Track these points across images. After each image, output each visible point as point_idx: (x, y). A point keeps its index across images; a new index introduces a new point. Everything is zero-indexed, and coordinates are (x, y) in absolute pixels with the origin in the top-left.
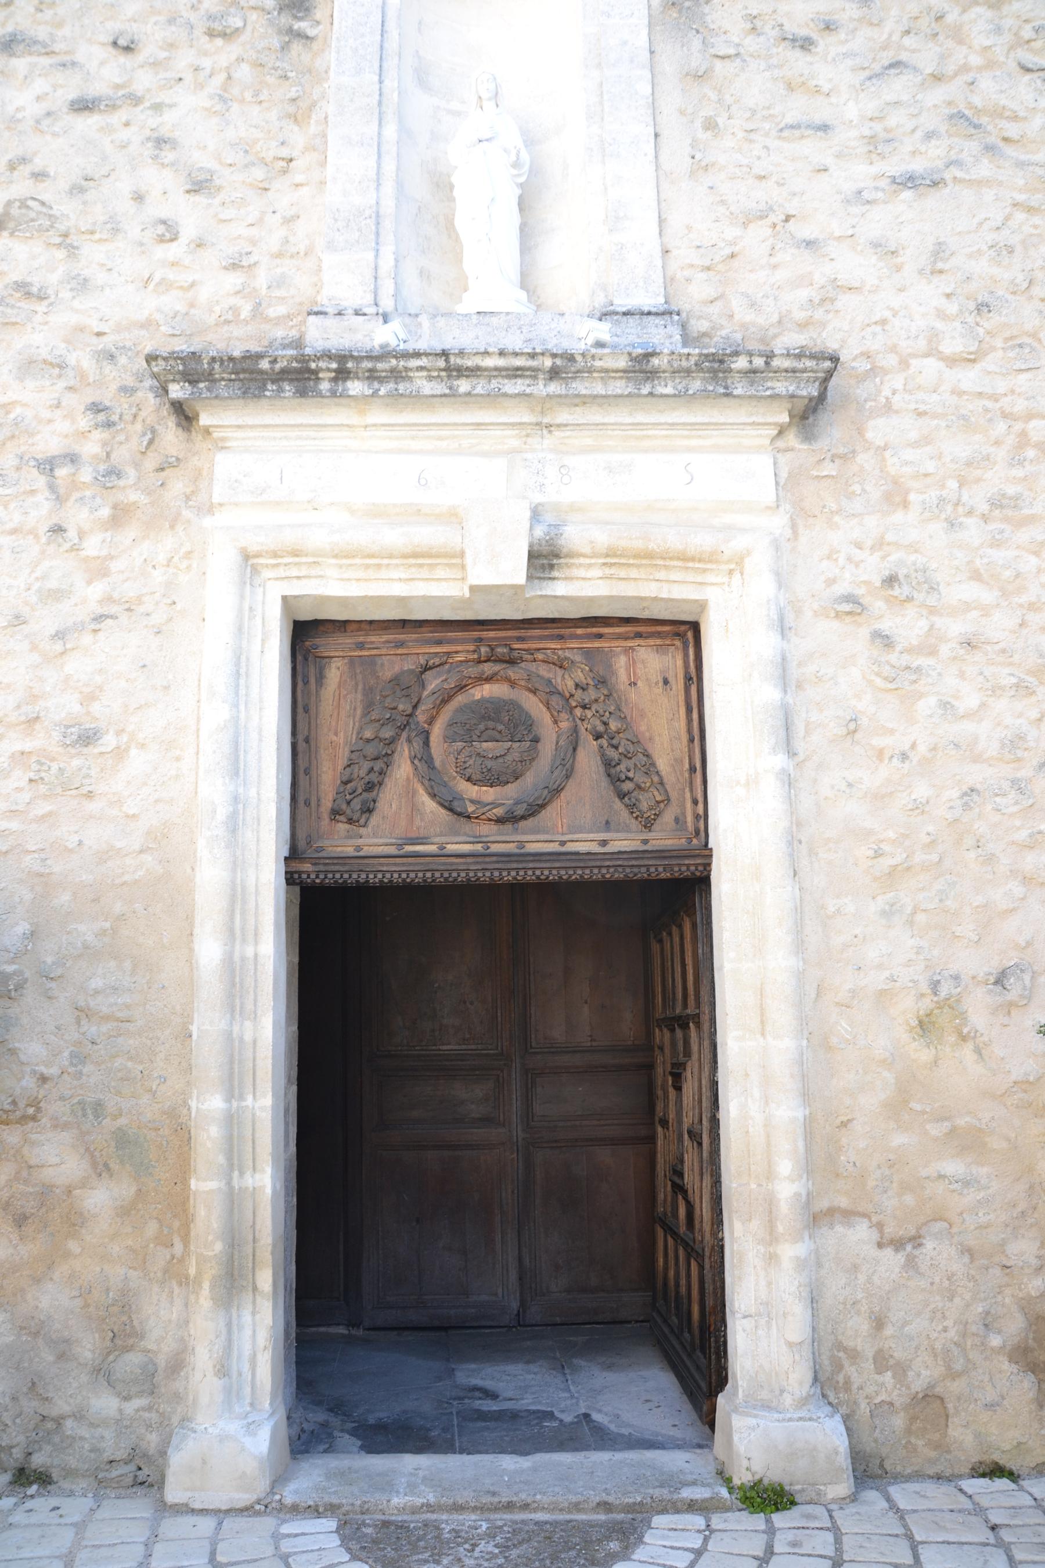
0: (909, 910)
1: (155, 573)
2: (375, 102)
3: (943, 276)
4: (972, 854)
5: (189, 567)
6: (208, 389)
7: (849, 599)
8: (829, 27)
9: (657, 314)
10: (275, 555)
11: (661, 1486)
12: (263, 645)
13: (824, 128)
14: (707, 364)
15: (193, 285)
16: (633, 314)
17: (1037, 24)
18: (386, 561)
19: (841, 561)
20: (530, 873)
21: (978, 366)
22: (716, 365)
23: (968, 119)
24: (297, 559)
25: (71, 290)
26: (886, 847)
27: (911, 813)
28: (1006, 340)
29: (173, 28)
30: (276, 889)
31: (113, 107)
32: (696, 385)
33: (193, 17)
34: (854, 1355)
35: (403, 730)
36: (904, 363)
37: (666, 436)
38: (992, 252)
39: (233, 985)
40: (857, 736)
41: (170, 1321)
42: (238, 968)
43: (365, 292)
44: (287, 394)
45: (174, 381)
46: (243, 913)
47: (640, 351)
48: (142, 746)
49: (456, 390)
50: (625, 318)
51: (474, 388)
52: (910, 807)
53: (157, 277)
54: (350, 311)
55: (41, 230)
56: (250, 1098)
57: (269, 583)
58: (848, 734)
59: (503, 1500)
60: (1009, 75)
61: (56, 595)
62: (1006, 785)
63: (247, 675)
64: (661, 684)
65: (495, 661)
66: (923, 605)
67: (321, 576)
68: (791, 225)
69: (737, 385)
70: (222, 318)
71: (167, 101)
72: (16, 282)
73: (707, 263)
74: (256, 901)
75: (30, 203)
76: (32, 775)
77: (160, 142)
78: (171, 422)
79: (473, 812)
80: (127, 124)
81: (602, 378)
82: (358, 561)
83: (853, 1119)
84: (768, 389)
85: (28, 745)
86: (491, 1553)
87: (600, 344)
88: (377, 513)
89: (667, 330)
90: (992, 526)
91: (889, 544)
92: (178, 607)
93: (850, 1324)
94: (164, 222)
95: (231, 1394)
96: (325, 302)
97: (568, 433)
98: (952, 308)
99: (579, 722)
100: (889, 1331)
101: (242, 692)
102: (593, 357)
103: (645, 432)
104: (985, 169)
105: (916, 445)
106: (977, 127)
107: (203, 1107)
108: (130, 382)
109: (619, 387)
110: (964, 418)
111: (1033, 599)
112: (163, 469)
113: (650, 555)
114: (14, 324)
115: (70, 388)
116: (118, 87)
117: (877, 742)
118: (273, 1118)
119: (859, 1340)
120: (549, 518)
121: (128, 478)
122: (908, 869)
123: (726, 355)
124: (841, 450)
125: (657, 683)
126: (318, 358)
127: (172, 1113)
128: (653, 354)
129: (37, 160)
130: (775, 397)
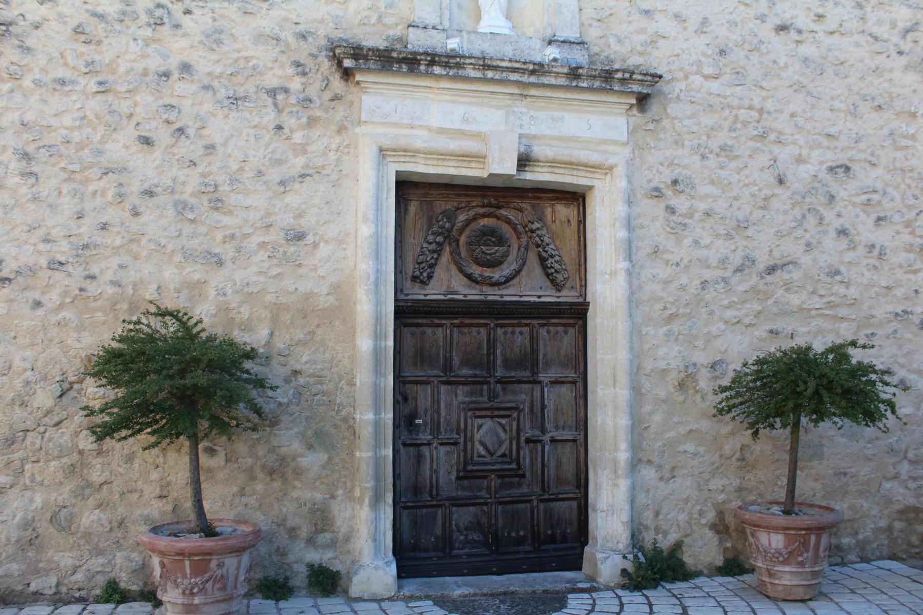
0: (676, 334)
1: (331, 154)
3: (705, 35)
4: (704, 310)
5: (348, 153)
7: (657, 189)
10: (395, 150)
18: (448, 157)
21: (718, 81)
24: (405, 153)
26: (668, 305)
28: (732, 69)
32: (597, 84)
34: (647, 528)
36: (686, 77)
40: (658, 254)
41: (345, 518)
47: (574, 65)
48: (327, 242)
50: (562, 45)
51: (494, 75)
54: (430, 27)
61: (280, 162)
62: (720, 279)
66: (689, 194)
73: (599, 18)
85: (266, 239)
87: (555, 60)
88: (442, 131)
92: (344, 172)
93: (645, 514)
98: (709, 52)
100: (661, 517)
102: (552, 66)
105: (689, 117)
108: (315, 51)
109: (562, 81)
110: (711, 106)
111: (736, 195)
113: (571, 164)
115: (282, 52)
117: (667, 257)
122: (677, 315)
124: (656, 118)
127: (345, 420)
128: (581, 68)
130: (632, 92)
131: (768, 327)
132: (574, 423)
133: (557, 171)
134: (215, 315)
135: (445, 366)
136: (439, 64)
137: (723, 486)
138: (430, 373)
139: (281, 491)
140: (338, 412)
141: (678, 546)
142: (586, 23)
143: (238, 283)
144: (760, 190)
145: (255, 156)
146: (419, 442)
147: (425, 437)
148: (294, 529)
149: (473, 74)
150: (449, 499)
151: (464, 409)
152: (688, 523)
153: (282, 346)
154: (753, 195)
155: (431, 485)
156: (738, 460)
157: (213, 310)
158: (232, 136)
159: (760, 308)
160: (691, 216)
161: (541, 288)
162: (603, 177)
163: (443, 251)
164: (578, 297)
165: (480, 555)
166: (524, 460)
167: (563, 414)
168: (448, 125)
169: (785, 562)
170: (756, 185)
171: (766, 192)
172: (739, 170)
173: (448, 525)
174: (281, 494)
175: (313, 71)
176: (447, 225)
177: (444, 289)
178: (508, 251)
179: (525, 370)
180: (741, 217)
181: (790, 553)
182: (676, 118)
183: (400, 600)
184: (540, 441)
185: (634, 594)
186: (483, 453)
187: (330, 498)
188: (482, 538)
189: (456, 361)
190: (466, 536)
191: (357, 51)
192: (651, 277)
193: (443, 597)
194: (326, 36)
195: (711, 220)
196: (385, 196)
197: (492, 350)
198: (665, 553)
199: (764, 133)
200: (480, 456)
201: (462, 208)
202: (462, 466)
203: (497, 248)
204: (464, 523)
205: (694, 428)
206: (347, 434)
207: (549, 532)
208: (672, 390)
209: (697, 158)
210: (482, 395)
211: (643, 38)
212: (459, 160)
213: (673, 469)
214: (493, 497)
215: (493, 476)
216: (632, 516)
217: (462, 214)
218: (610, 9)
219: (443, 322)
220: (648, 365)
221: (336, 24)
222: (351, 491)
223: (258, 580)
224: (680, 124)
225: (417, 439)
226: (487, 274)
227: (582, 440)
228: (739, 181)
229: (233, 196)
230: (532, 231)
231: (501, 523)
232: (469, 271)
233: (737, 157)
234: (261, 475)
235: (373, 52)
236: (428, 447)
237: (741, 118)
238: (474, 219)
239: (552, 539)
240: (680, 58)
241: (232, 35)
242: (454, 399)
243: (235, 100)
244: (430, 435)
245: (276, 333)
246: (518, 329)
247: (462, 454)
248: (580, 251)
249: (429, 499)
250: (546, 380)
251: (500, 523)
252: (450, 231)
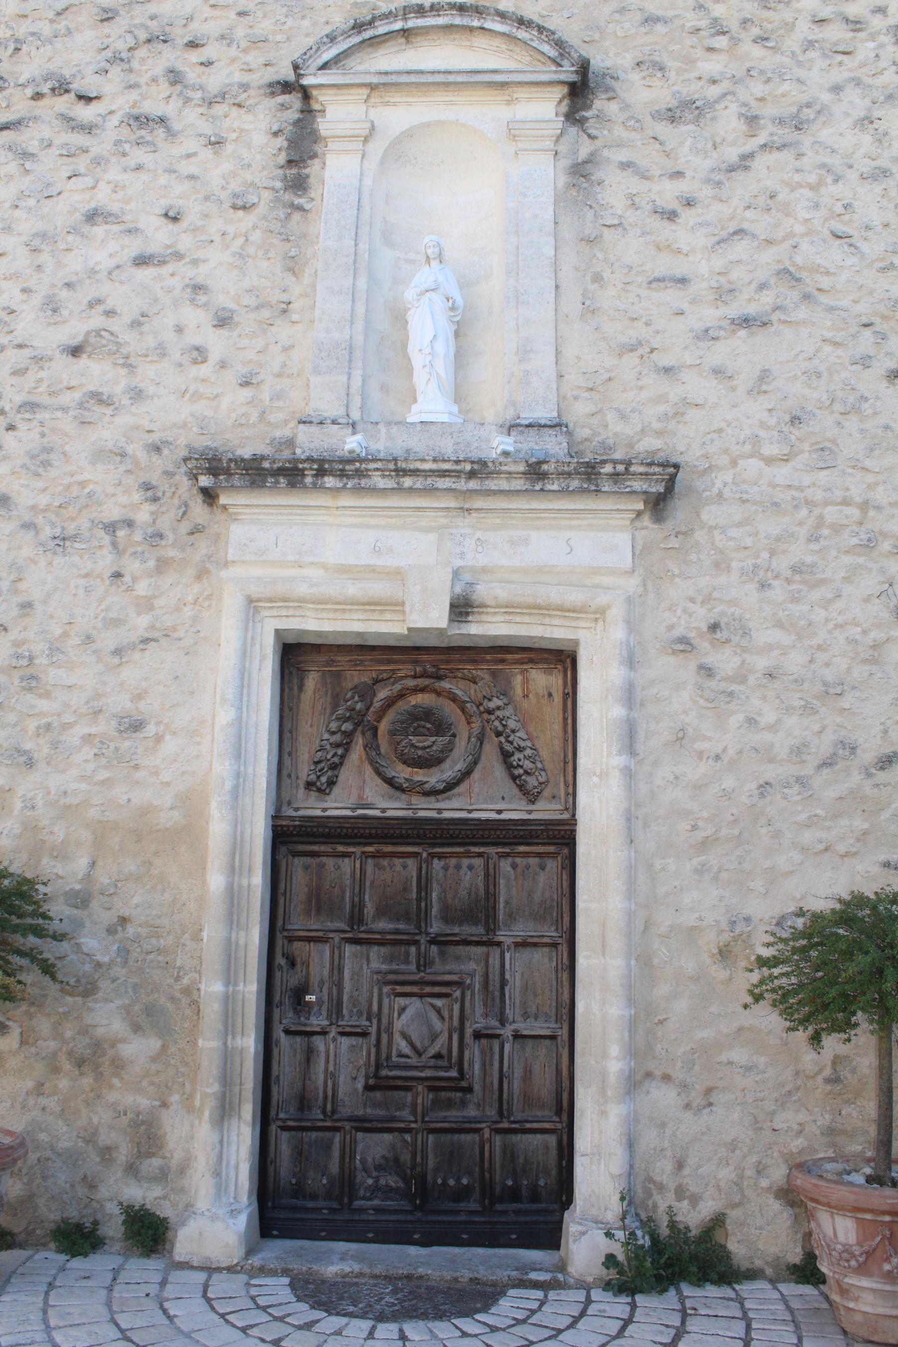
0: (715, 869)
1: (186, 609)
2: (352, 261)
4: (764, 831)
5: (210, 606)
6: (227, 480)
7: (683, 640)
8: (689, 203)
9: (550, 426)
13: (682, 281)
15: (217, 396)
17: (845, 202)
18: (349, 607)
19: (679, 613)
21: (790, 464)
22: (590, 470)
23: (791, 274)
25: (131, 398)
26: (700, 823)
28: (812, 445)
29: (208, 204)
30: (265, 839)
31: (162, 263)
32: (575, 484)
33: (224, 195)
34: (661, 1187)
36: (734, 463)
37: (555, 518)
38: (804, 377)
39: (232, 905)
40: (684, 742)
41: (181, 1138)
47: (534, 460)
48: (174, 733)
50: (527, 430)
51: (414, 483)
53: (191, 391)
54: (329, 421)
55: (111, 353)
56: (242, 984)
60: (824, 240)
61: (115, 623)
63: (249, 686)
68: (654, 356)
71: (202, 257)
72: (91, 392)
73: (591, 386)
75: (103, 333)
76: (96, 751)
77: (198, 288)
78: (199, 499)
80: (172, 275)
82: (328, 606)
85: (93, 730)
87: (506, 454)
88: (343, 570)
90: (793, 587)
92: (202, 634)
94: (197, 349)
95: (220, 1189)
96: (311, 413)
98: (773, 421)
100: (687, 1171)
101: (245, 699)
102: (500, 463)
104: (802, 313)
105: (739, 525)
106: (798, 280)
108: (171, 468)
109: (519, 484)
110: (776, 504)
111: (821, 642)
112: (192, 533)
113: (538, 607)
114: (90, 423)
115: (129, 472)
116: (168, 247)
117: (700, 746)
118: (258, 1000)
120: (467, 577)
122: (717, 839)
124: (684, 529)
129: (108, 301)
130: (633, 492)
131: (882, 858)
132: (554, 1009)
133: (518, 619)
134: (20, 836)
135: (352, 917)
136: (331, 473)
137: (800, 1124)
138: (330, 925)
139: (92, 1090)
140: (178, 979)
141: (718, 1221)
142: (569, 395)
143: (53, 792)
144: (865, 632)
145: (83, 616)
146: (308, 1029)
147: (318, 1021)
148: (108, 1149)
149: (381, 483)
150: (350, 1119)
151: (378, 981)
152: (736, 1184)
153: (106, 881)
154: (852, 641)
156: (828, 1081)
157: (17, 830)
158: (56, 589)
159: (866, 826)
160: (742, 679)
161: (503, 798)
162: (592, 625)
163: (353, 745)
164: (561, 812)
165: (396, 1212)
166: (471, 1063)
167: (536, 996)
168: (352, 561)
169: (862, 1270)
170: (857, 625)
171: (876, 635)
172: (826, 604)
173: (347, 1160)
174: (92, 1095)
175: (168, 494)
176: (359, 706)
177: (353, 800)
178: (451, 742)
179: (476, 924)
180: (829, 678)
181: (869, 1254)
182: (716, 527)
184: (498, 1036)
186: (405, 1048)
188: (401, 1185)
189: (370, 908)
190: (377, 1179)
191: (214, 464)
192: (672, 778)
193: (311, 1274)
194: (188, 446)
195: (777, 684)
196: (256, 665)
197: (423, 894)
198: (694, 1233)
199: (869, 540)
200: (401, 1055)
201: (383, 680)
202: (372, 1069)
203: (433, 739)
204: (374, 1159)
205: (747, 1025)
206: (188, 1012)
207: (510, 1183)
208: (708, 961)
209: (752, 587)
210: (407, 962)
211: (661, 408)
212: (366, 611)
213: (709, 1091)
214: (419, 1119)
215: (420, 1088)
216: (631, 1166)
218: (608, 371)
219: (351, 849)
220: (665, 920)
222: (190, 1098)
223: (53, 1221)
224: (722, 536)
225: (305, 1025)
226: (417, 778)
227: (566, 1037)
228: (827, 620)
229: (52, 671)
230: (490, 712)
231: (431, 1163)
232: (390, 773)
233: (823, 582)
234: (67, 1066)
236: (322, 1037)
237: (829, 519)
238: (401, 696)
239: (514, 1195)
240: (723, 435)
241: (64, 454)
242: (365, 966)
243: (62, 540)
245: (100, 863)
246: (465, 862)
247: (373, 1050)
249: (321, 1117)
250: (508, 941)
252: (363, 714)
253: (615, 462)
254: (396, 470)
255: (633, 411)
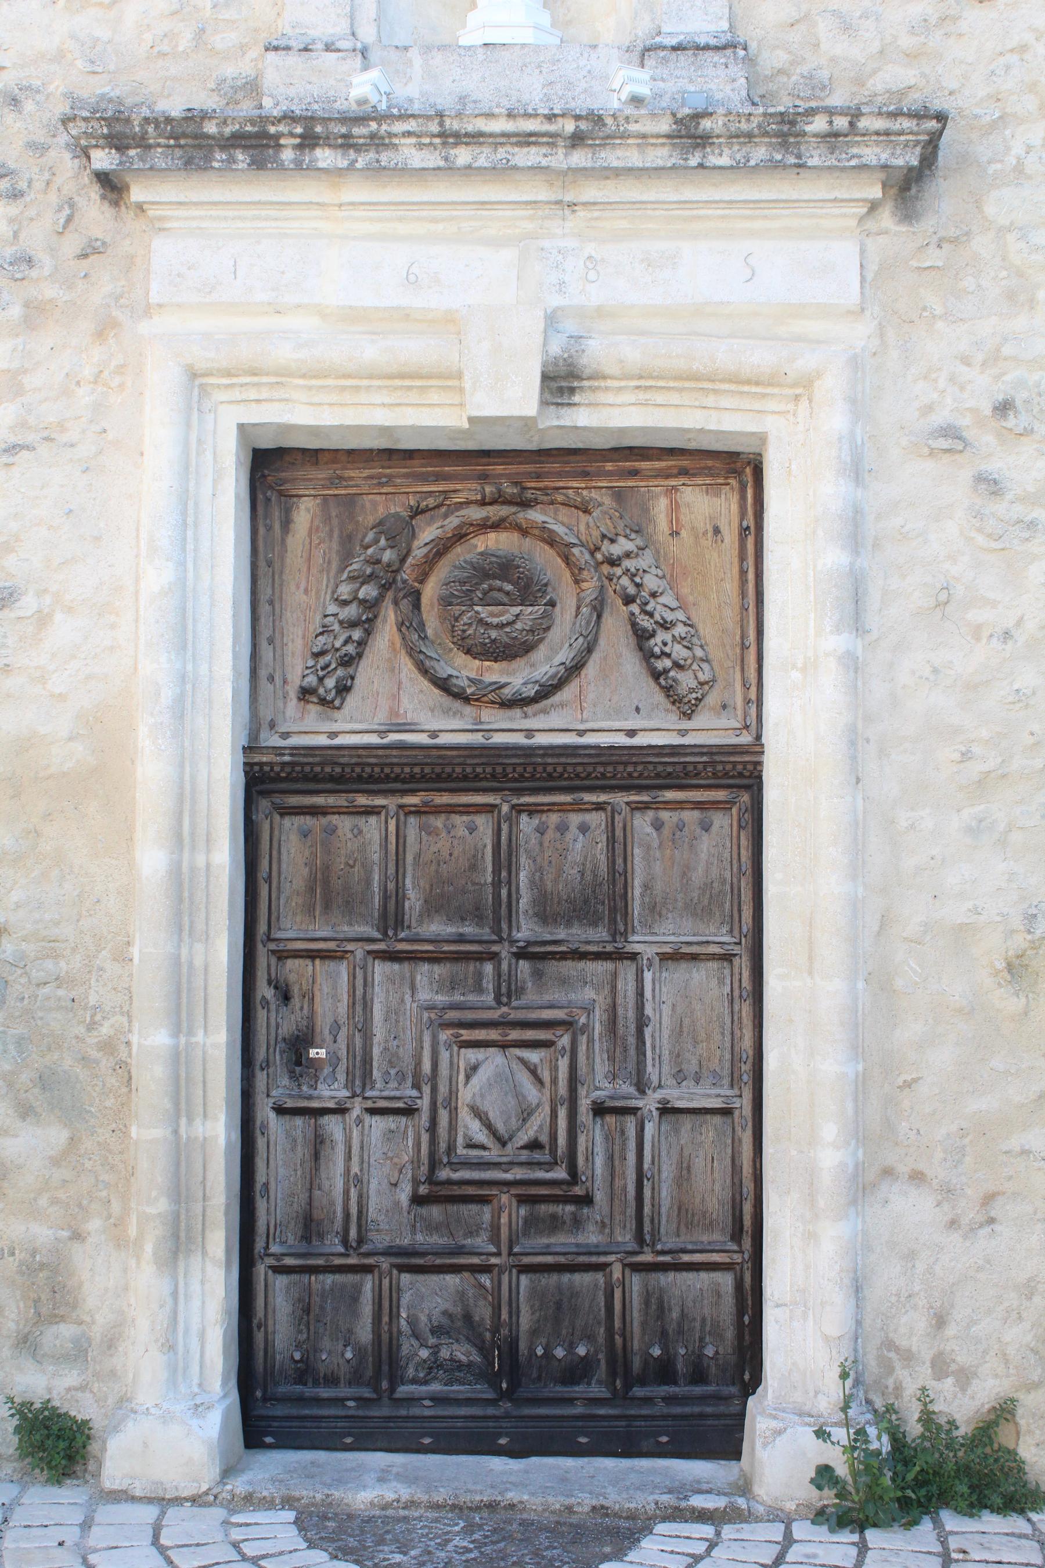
5: (122, 386)
6: (142, 159)
7: (949, 432)
9: (717, 48)
11: (670, 1492)
12: (214, 487)
14: (774, 127)
16: (685, 49)
18: (365, 382)
20: (540, 769)
22: (786, 128)
24: (256, 379)
26: (976, 749)
27: (1011, 706)
32: (760, 153)
34: (908, 1357)
35: (388, 589)
37: (723, 217)
39: (180, 900)
40: (949, 608)
41: (106, 1290)
42: (187, 880)
43: (338, 16)
44: (241, 166)
45: (97, 146)
46: (193, 814)
47: (687, 111)
48: (70, 610)
49: (453, 162)
50: (674, 54)
51: (475, 159)
52: (1011, 699)
54: (320, 46)
57: (222, 408)
58: (938, 605)
59: (485, 1499)
63: (196, 525)
64: (710, 534)
65: (504, 503)
67: (286, 400)
69: (814, 153)
70: (156, 50)
74: (209, 800)
78: (95, 191)
79: (473, 694)
81: (638, 145)
83: (919, 1078)
84: (853, 157)
86: (465, 1547)
87: (636, 100)
89: (728, 71)
91: (1005, 359)
92: (110, 436)
93: (904, 1319)
96: (288, 31)
97: (596, 214)
99: (606, 582)
100: (951, 1331)
101: (190, 546)
102: (627, 119)
103: (695, 212)
107: (146, 1043)
108: (40, 136)
109: (661, 156)
112: (85, 256)
113: (696, 377)
117: (975, 615)
119: (915, 1339)
120: (570, 326)
121: (42, 267)
122: (1004, 776)
123: (799, 114)
124: (952, 232)
125: (705, 533)
126: (280, 120)
127: (108, 1046)
128: (707, 114)
130: (863, 167)
133: (660, 398)
136: (327, 140)
138: (347, 930)
140: (92, 1026)
146: (315, 1104)
150: (388, 1252)
151: (431, 1021)
155: (347, 1215)
161: (638, 710)
162: (791, 407)
165: (469, 1402)
167: (696, 1042)
173: (386, 1319)
175: (38, 185)
176: (387, 556)
177: (381, 717)
179: (594, 924)
183: (222, 1505)
184: (633, 1111)
185: (835, 1538)
186: (481, 1136)
187: (71, 1239)
188: (476, 1358)
189: (414, 900)
190: (436, 1349)
191: (118, 128)
194: (69, 96)
196: (207, 489)
197: (504, 874)
198: (964, 1430)
202: (424, 1169)
203: (516, 610)
206: (112, 1081)
207: (656, 1352)
210: (479, 989)
212: (396, 388)
213: (989, 1199)
214: (504, 1250)
215: (504, 1198)
216: (859, 1323)
217: (429, 524)
219: (379, 801)
221: (93, 62)
222: (120, 1223)
225: (310, 1098)
227: (747, 1110)
230: (613, 562)
232: (443, 670)
235: (157, 127)
238: (459, 536)
242: (408, 998)
244: (346, 1087)
247: (425, 1138)
248: (744, 609)
249: (342, 1250)
250: (648, 951)
251: (525, 1321)
253: (831, 112)
254: (442, 135)
255: (865, 16)
